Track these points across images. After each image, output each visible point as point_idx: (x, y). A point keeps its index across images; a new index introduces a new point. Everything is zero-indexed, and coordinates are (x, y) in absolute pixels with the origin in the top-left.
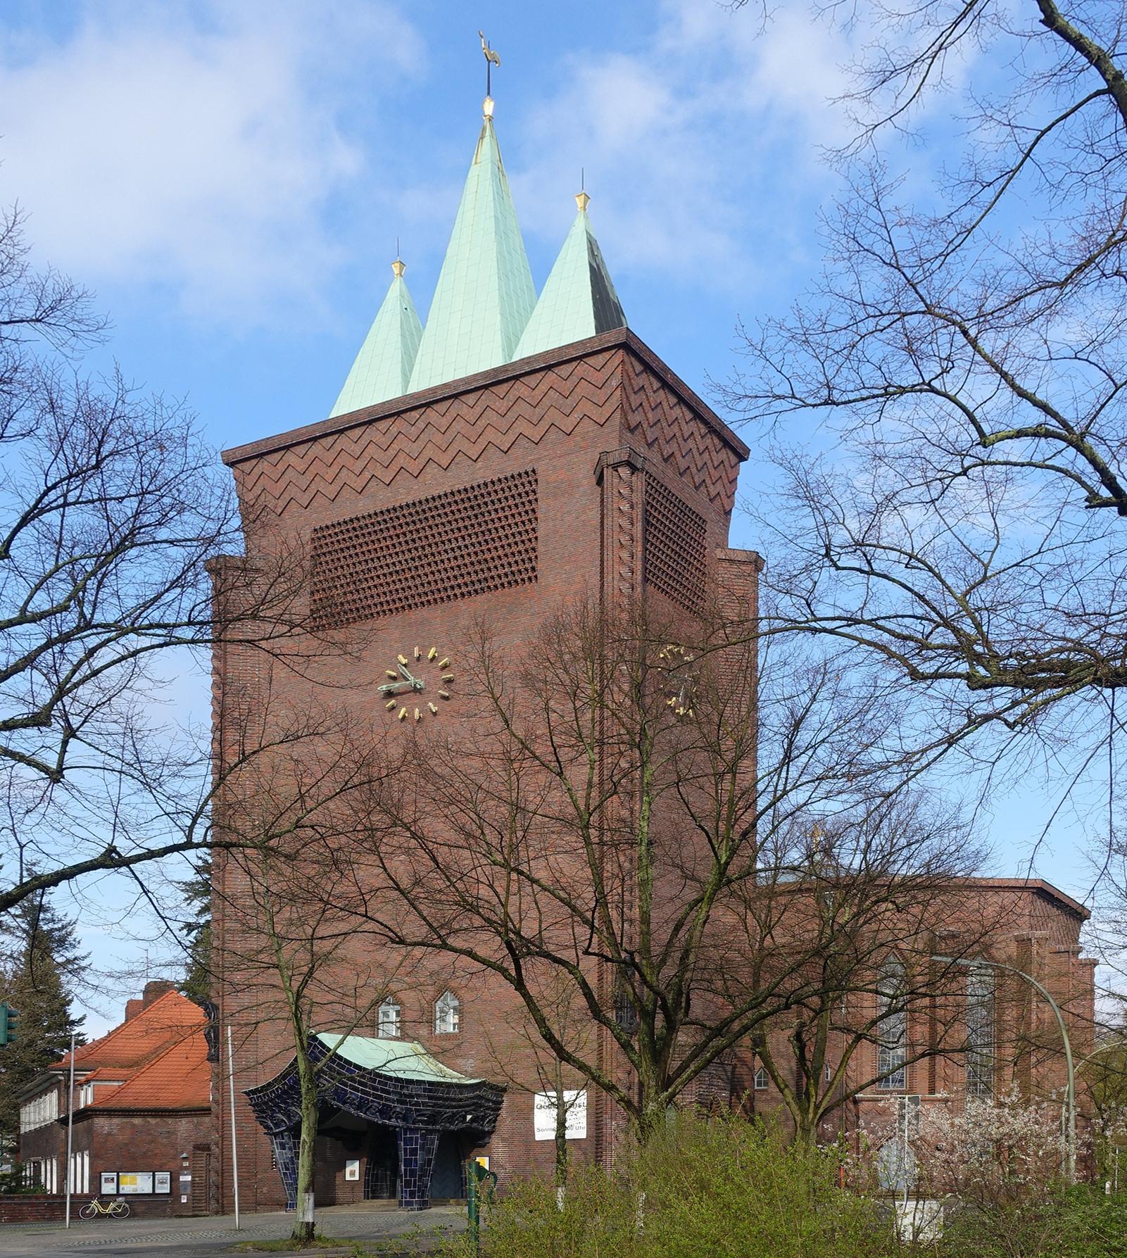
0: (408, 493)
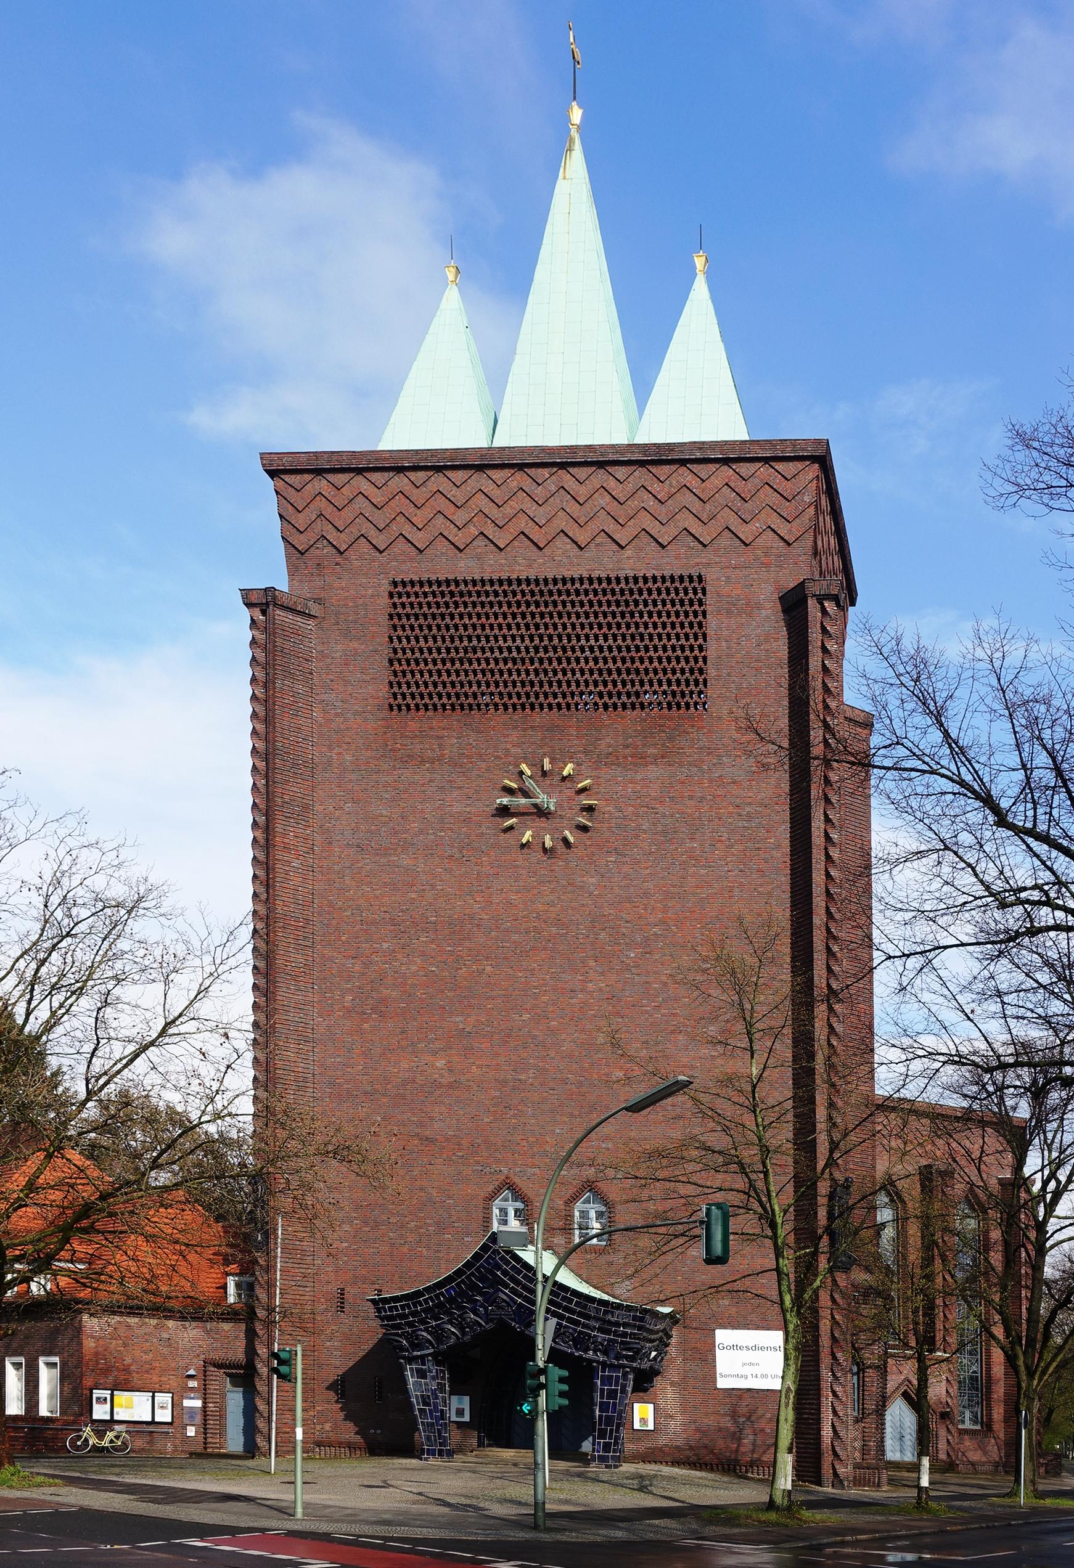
0: (530, 566)
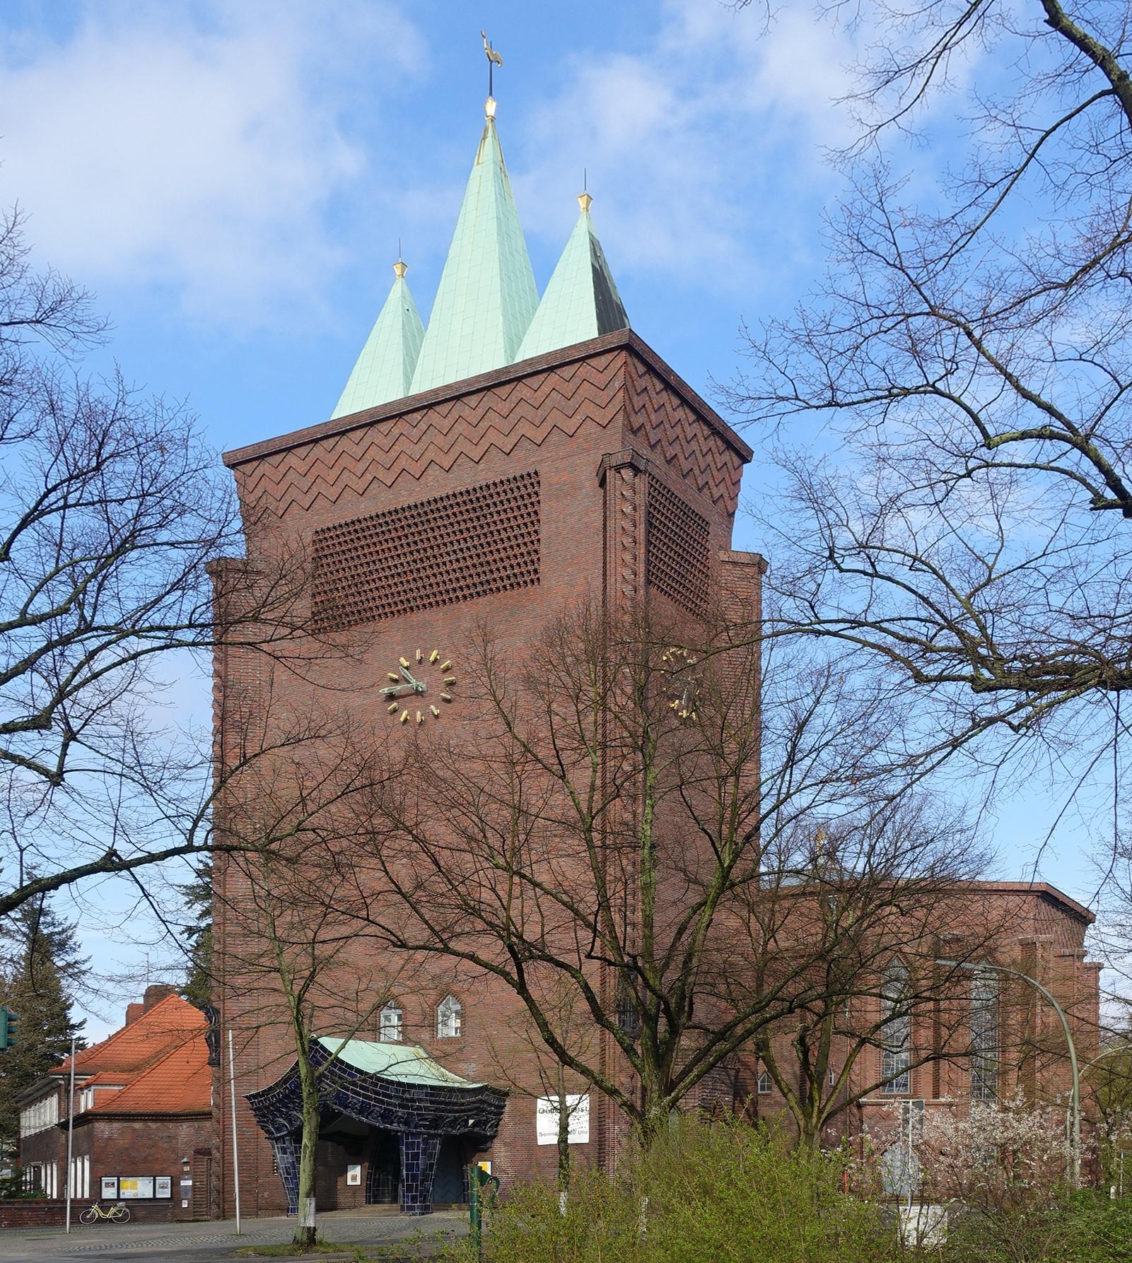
0: (410, 495)
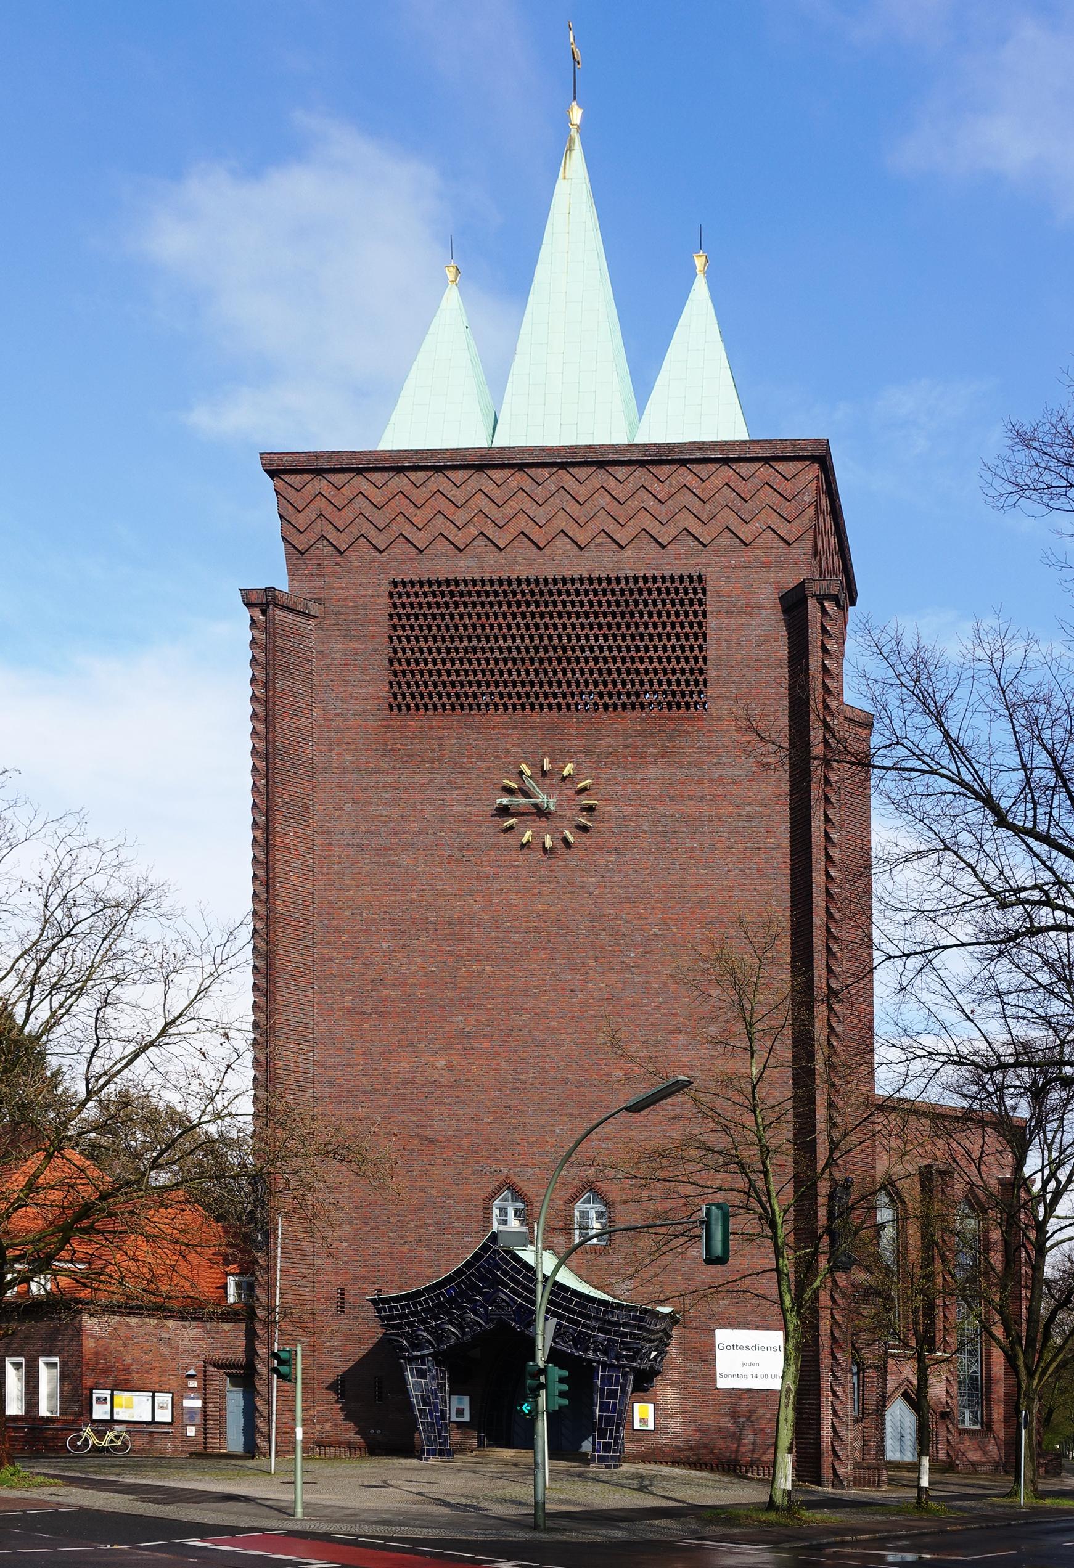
0: (530, 566)
